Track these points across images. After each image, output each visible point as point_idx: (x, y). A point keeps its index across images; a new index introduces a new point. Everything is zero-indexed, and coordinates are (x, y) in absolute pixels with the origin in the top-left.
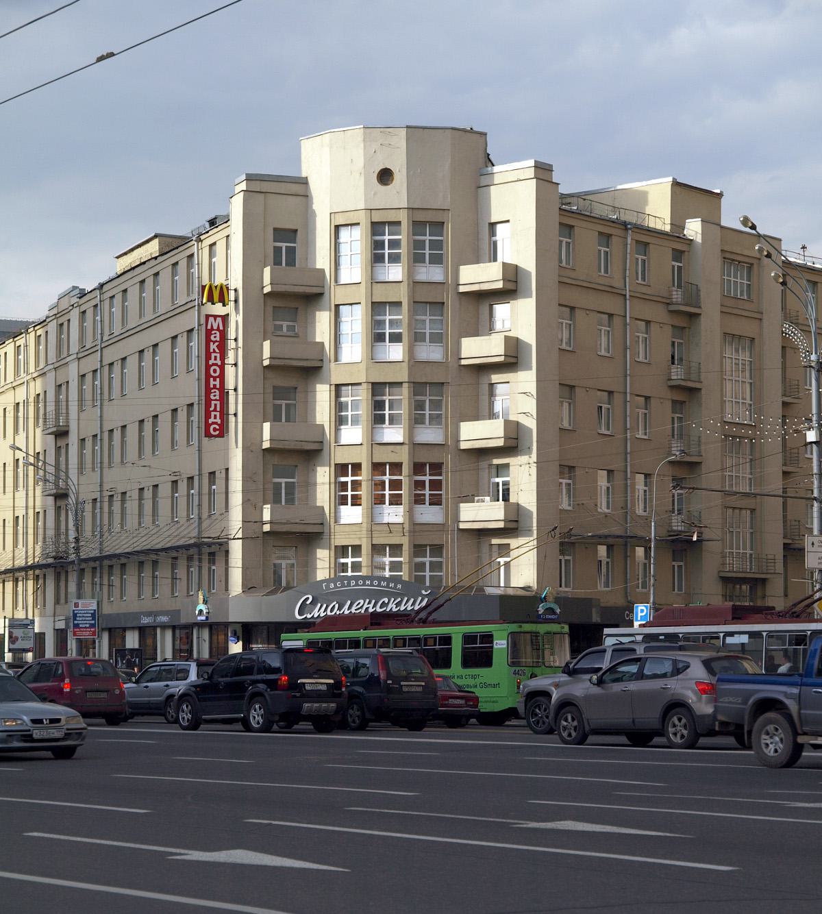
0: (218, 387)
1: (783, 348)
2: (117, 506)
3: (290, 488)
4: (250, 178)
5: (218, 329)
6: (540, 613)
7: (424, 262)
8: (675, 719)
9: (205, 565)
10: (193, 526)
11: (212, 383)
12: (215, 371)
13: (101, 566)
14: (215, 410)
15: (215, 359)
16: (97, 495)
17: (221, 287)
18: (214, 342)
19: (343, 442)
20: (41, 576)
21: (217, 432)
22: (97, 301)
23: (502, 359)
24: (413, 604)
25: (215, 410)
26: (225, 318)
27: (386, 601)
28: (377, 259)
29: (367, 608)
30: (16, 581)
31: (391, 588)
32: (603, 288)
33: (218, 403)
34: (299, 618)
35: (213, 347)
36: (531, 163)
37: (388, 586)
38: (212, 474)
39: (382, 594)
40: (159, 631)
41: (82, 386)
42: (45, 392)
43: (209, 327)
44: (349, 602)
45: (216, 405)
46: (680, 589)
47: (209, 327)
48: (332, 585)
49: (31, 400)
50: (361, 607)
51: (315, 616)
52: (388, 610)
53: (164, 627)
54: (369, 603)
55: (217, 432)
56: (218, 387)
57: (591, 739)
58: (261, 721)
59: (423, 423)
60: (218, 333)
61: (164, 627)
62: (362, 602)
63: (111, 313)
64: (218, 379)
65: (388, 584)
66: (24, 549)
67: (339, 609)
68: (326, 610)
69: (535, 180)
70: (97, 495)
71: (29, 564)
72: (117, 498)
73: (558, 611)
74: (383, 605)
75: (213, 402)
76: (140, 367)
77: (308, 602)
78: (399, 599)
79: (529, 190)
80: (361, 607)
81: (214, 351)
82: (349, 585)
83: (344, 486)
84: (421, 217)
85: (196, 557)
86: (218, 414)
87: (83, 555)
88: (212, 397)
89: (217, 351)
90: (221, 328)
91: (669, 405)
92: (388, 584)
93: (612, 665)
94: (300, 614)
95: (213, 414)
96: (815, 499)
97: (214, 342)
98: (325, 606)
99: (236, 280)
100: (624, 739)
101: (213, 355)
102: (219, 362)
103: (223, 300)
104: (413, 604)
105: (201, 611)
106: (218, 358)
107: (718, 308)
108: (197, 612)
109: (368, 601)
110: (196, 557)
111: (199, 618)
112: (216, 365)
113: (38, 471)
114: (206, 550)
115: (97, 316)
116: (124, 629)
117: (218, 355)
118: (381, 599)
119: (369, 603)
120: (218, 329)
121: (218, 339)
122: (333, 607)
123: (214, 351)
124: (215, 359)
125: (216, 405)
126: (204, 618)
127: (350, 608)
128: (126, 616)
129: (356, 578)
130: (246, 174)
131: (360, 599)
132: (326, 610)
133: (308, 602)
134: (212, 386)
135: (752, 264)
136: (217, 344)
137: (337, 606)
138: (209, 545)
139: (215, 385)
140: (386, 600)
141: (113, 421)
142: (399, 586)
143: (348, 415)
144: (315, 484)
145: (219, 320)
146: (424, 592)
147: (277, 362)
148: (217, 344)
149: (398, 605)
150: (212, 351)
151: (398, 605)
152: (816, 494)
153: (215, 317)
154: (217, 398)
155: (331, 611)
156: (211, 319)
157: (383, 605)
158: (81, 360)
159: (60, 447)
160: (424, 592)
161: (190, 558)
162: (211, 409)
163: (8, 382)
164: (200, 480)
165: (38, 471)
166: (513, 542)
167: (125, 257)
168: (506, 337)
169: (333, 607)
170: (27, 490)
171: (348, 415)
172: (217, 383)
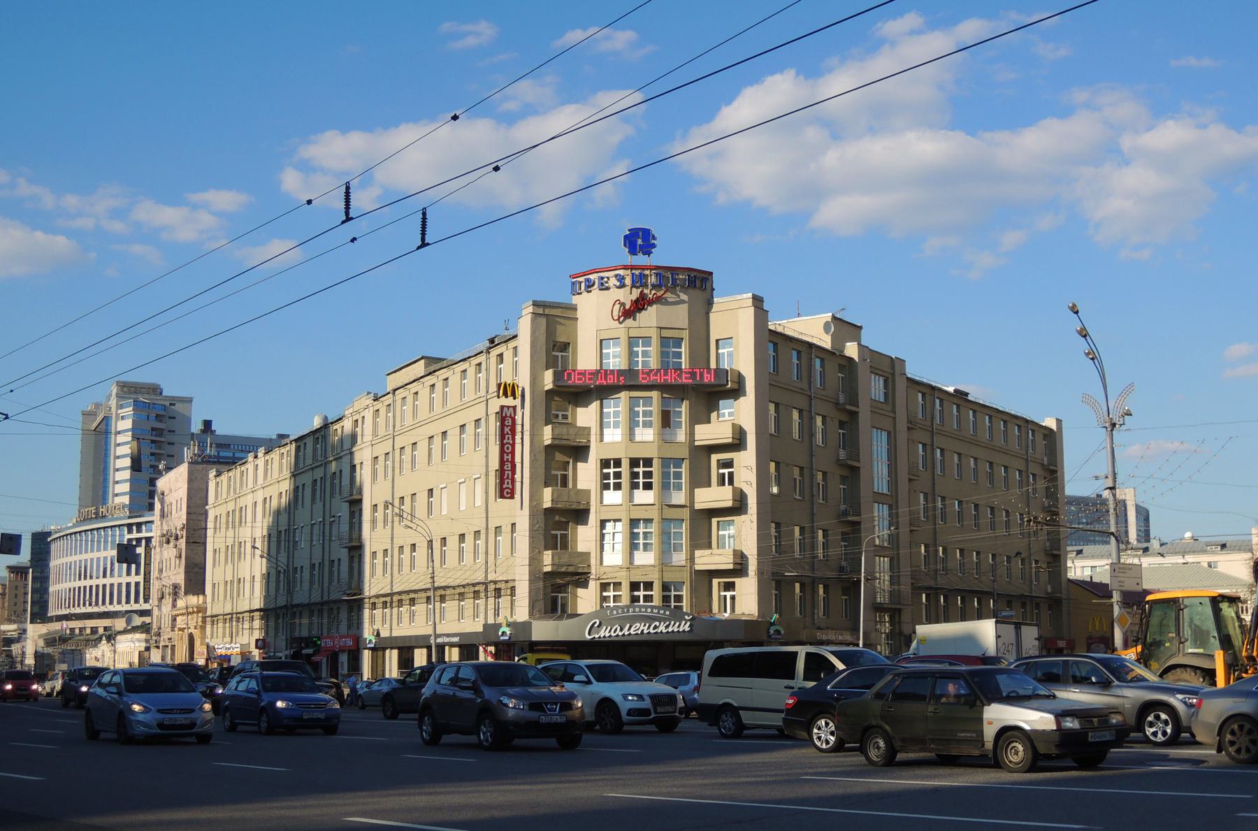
0: (510, 460)
1: (908, 439)
2: (406, 556)
3: (564, 537)
4: (535, 304)
5: (510, 416)
6: (771, 634)
7: (610, 427)
8: (724, 716)
9: (491, 600)
10: (314, 595)
11: (506, 457)
12: (508, 448)
13: (486, 590)
14: (508, 478)
15: (508, 439)
16: (388, 546)
17: (513, 385)
18: (507, 426)
19: (605, 502)
20: (298, 613)
21: (509, 495)
22: (390, 401)
23: (730, 440)
24: (679, 626)
25: (508, 478)
26: (514, 408)
27: (658, 625)
28: (633, 547)
29: (643, 630)
30: (277, 617)
31: (661, 614)
32: (798, 390)
33: (510, 473)
34: (589, 637)
35: (507, 430)
36: (750, 295)
37: (658, 613)
38: (401, 548)
39: (653, 619)
40: (447, 648)
41: (374, 465)
42: (341, 471)
43: (504, 415)
44: (628, 625)
45: (508, 474)
46: (846, 617)
47: (504, 415)
48: (615, 612)
49: (237, 510)
50: (638, 629)
51: (602, 636)
52: (659, 631)
53: (452, 645)
54: (645, 626)
55: (509, 495)
56: (510, 460)
57: (401, 716)
58: (733, 728)
59: (609, 489)
60: (510, 419)
61: (452, 645)
62: (638, 625)
63: (402, 412)
64: (510, 455)
65: (659, 611)
66: (320, 589)
67: (621, 630)
68: (610, 631)
69: (753, 308)
70: (388, 546)
71: (324, 600)
72: (407, 550)
73: (783, 632)
74: (655, 627)
75: (506, 472)
76: (430, 450)
77: (596, 625)
78: (668, 623)
79: (747, 317)
80: (638, 629)
81: (508, 434)
82: (628, 611)
83: (607, 476)
84: (666, 333)
85: (482, 595)
86: (510, 481)
87: (436, 585)
88: (506, 468)
89: (510, 433)
90: (513, 415)
91: (838, 479)
92: (659, 611)
93: (546, 678)
94: (589, 634)
95: (506, 481)
96: (1112, 534)
97: (507, 426)
98: (609, 628)
99: (524, 381)
100: (653, 728)
101: (507, 436)
102: (511, 442)
103: (514, 395)
104: (679, 626)
105: (504, 633)
106: (510, 439)
107: (869, 409)
108: (500, 634)
109: (643, 624)
110: (482, 595)
111: (502, 638)
112: (509, 443)
113: (412, 512)
114: (492, 587)
115: (389, 412)
116: (414, 648)
117: (510, 436)
118: (653, 623)
119: (645, 626)
120: (510, 416)
121: (510, 424)
122: (616, 629)
123: (508, 434)
124: (508, 439)
125: (508, 474)
126: (507, 638)
127: (629, 629)
128: (417, 637)
129: (646, 607)
130: (533, 301)
131: (636, 623)
132: (610, 631)
133: (596, 625)
134: (505, 460)
135: (888, 378)
136: (509, 428)
137: (619, 628)
138: (495, 582)
139: (507, 459)
140: (657, 623)
141: (403, 489)
142: (668, 613)
143: (614, 479)
144: (747, 504)
145: (511, 409)
146: (686, 617)
147: (556, 442)
148: (509, 428)
149: (667, 627)
150: (505, 433)
151: (667, 627)
152: (1113, 529)
153: (508, 407)
154: (509, 469)
155: (615, 632)
156: (506, 409)
157: (655, 627)
158: (297, 477)
159: (354, 511)
160: (686, 617)
161: (476, 594)
162: (505, 477)
163: (248, 488)
164: (487, 534)
165: (412, 512)
166: (737, 581)
167: (394, 374)
168: (733, 424)
169: (616, 629)
170: (234, 565)
171: (614, 479)
172: (510, 457)
